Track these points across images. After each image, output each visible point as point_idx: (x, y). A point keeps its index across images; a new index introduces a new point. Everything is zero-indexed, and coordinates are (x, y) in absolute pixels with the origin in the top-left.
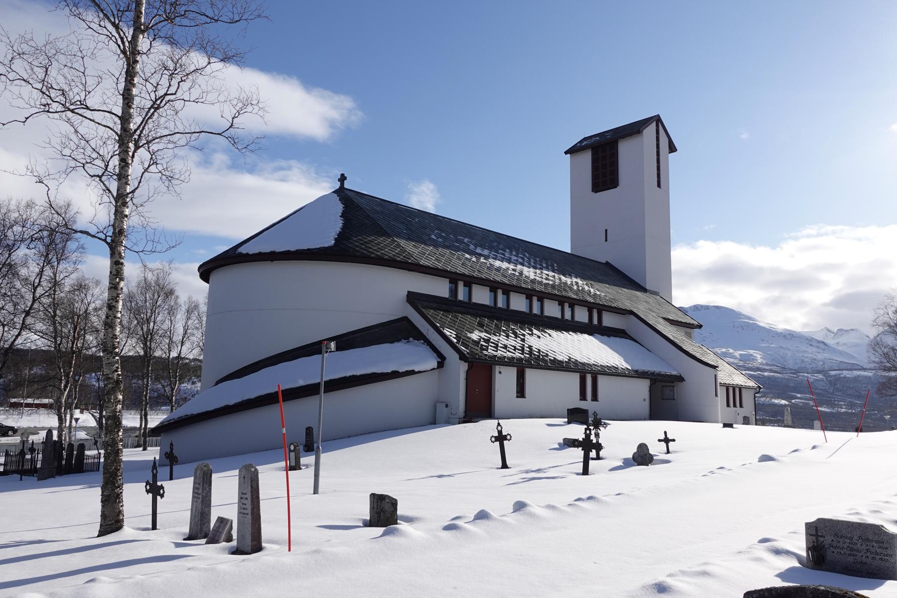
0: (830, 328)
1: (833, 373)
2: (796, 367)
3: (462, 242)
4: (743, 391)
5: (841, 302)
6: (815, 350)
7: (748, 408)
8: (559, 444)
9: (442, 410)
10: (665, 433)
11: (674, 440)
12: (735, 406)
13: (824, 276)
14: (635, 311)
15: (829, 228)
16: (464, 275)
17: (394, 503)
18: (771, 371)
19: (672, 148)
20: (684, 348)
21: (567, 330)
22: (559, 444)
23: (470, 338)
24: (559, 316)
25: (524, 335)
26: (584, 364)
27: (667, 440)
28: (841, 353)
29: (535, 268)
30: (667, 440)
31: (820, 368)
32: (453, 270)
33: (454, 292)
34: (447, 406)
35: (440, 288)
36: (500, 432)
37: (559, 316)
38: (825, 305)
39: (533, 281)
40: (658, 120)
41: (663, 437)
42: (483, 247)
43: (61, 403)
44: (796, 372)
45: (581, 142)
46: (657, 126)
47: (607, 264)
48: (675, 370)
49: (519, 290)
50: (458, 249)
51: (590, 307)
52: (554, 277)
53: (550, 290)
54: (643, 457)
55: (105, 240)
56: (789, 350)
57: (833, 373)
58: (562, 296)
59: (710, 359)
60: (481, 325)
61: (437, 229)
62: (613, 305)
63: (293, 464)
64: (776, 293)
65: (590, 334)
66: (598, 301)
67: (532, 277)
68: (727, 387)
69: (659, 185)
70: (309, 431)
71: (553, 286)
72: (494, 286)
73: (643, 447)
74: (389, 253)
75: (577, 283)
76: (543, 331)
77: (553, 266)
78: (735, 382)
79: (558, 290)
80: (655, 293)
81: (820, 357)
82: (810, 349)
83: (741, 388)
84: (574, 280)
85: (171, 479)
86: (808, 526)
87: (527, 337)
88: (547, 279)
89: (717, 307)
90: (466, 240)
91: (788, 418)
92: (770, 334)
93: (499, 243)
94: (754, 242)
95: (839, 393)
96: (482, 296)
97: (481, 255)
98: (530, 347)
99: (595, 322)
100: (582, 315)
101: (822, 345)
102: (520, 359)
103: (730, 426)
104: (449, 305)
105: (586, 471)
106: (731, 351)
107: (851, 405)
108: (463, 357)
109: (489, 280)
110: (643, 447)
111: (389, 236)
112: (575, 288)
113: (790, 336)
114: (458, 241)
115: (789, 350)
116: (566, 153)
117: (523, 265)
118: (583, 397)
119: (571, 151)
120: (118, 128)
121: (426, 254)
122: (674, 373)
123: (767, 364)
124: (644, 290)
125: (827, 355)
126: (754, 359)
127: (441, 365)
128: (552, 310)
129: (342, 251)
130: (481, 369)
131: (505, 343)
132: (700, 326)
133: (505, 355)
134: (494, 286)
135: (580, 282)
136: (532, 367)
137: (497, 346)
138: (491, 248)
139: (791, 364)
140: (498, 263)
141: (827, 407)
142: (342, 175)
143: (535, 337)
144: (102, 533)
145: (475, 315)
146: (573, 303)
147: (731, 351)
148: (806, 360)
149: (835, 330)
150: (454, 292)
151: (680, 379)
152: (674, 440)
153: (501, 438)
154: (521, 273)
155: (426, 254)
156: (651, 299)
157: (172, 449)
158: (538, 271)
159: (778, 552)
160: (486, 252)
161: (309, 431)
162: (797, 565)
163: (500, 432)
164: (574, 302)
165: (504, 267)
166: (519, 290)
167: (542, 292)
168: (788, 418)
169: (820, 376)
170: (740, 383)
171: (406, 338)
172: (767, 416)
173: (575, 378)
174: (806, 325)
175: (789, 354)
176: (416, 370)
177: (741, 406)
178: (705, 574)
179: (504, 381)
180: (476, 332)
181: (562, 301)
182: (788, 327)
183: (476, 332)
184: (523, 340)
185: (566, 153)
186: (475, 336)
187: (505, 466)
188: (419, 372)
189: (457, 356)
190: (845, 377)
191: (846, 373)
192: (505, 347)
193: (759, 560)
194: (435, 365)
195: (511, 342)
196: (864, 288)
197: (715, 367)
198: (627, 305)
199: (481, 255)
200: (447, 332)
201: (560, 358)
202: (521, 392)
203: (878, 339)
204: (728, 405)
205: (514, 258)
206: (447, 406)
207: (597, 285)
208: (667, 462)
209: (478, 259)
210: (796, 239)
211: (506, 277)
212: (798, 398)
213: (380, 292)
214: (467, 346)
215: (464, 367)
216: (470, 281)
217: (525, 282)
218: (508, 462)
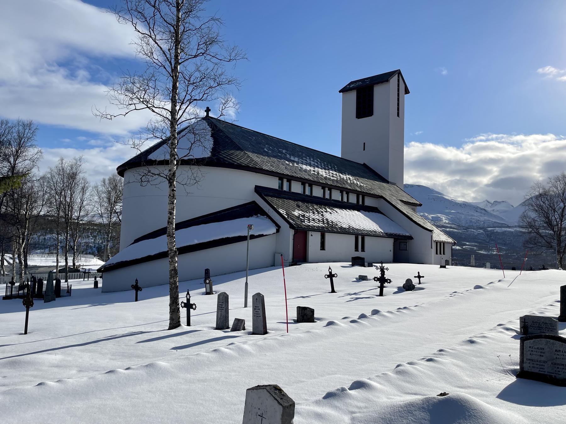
0: (489, 200)
1: (489, 229)
2: (467, 225)
3: (280, 152)
4: (445, 244)
5: (498, 183)
6: (479, 214)
7: (448, 255)
8: (356, 278)
9: (278, 258)
10: (419, 273)
11: (423, 277)
12: (440, 254)
13: (489, 167)
14: (384, 196)
15: (494, 136)
16: (288, 175)
17: (312, 311)
18: (451, 228)
19: (407, 91)
20: (414, 219)
21: (346, 209)
22: (356, 278)
23: (294, 215)
24: (340, 200)
25: (322, 212)
26: (357, 230)
27: (419, 277)
28: (495, 216)
29: (325, 169)
30: (419, 277)
31: (481, 226)
32: (282, 172)
33: (281, 186)
34: (282, 255)
35: (273, 183)
36: (331, 273)
37: (340, 200)
38: (487, 185)
39: (326, 178)
40: (399, 73)
41: (417, 275)
42: (295, 156)
43: (20, 252)
44: (467, 228)
45: (349, 84)
46: (398, 77)
47: (364, 165)
48: (408, 233)
49: (318, 184)
50: (281, 158)
51: (358, 193)
52: (336, 175)
53: (335, 184)
54: (409, 286)
55: (166, 178)
56: (463, 214)
57: (489, 229)
58: (343, 188)
59: (429, 226)
60: (298, 206)
61: (267, 144)
62: (372, 193)
63: (208, 291)
64: (457, 177)
65: (358, 211)
66: (363, 191)
67: (325, 176)
68: (437, 242)
69: (398, 115)
70: (207, 271)
71: (337, 181)
72: (304, 182)
73: (409, 281)
74: (244, 161)
75: (349, 178)
76: (332, 209)
77: (335, 168)
78: (441, 240)
79: (340, 184)
80: (394, 184)
81: (482, 219)
82: (476, 214)
83: (444, 243)
84: (348, 176)
85: (136, 300)
86: (521, 318)
87: (324, 213)
88: (333, 176)
89: (419, 186)
90: (284, 151)
91: (473, 261)
92: (453, 204)
93: (303, 153)
94: (446, 144)
95: (493, 242)
96: (297, 188)
97: (294, 161)
98: (327, 219)
99: (361, 203)
100: (353, 199)
101: (483, 211)
102: (323, 227)
103: (444, 267)
104: (279, 193)
105: (381, 294)
106: (426, 215)
107: (499, 250)
108: (291, 226)
109: (302, 178)
110: (409, 281)
111: (242, 150)
112: (349, 181)
113: (465, 205)
114: (280, 152)
115: (463, 214)
116: (340, 92)
117: (318, 168)
118: (357, 249)
119: (343, 91)
120: (170, 118)
121: (266, 163)
122: (407, 234)
123: (448, 223)
124: (387, 182)
125: (486, 218)
126: (441, 220)
127: (278, 231)
128: (336, 196)
129: (216, 160)
130: (301, 233)
131: (313, 217)
132: (421, 205)
133: (315, 225)
134: (304, 182)
135: (351, 178)
136: (330, 232)
137: (309, 220)
138: (299, 157)
139: (463, 224)
140: (304, 167)
141: (485, 251)
142: (208, 108)
143: (328, 213)
144: (171, 328)
145: (295, 200)
146: (348, 191)
147: (426, 215)
148: (473, 221)
149: (492, 202)
150: (281, 186)
151: (411, 238)
152: (423, 277)
153: (331, 276)
154: (318, 173)
155: (266, 163)
156: (392, 188)
157: (137, 283)
158: (327, 171)
159: (508, 329)
160: (296, 159)
161: (207, 271)
162: (516, 334)
163: (331, 273)
164: (349, 191)
165: (308, 169)
166: (318, 184)
167: (331, 185)
168: (473, 261)
169: (481, 231)
170: (444, 240)
171: (256, 215)
172: (461, 259)
173: (353, 238)
174: (474, 198)
175: (463, 216)
176: (265, 234)
177: (444, 254)
178: (484, 337)
179: (314, 239)
180: (297, 211)
181: (342, 190)
182: (463, 200)
183: (297, 211)
184: (322, 215)
185: (340, 92)
186: (296, 213)
187: (333, 291)
188: (266, 235)
189: (288, 226)
190: (497, 232)
191: (498, 230)
192: (314, 220)
193: (501, 332)
194: (275, 231)
195: (316, 217)
196: (512, 175)
197: (431, 231)
198: (379, 192)
199: (294, 161)
200: (281, 211)
201: (344, 226)
202: (323, 247)
203: (525, 213)
204: (437, 254)
205: (312, 163)
206: (282, 255)
207: (361, 180)
208: (422, 289)
209: (293, 164)
210: (473, 142)
211: (310, 176)
212: (467, 245)
213: (238, 186)
214: (293, 220)
215: (292, 232)
216: (290, 179)
217: (322, 179)
218: (335, 289)
